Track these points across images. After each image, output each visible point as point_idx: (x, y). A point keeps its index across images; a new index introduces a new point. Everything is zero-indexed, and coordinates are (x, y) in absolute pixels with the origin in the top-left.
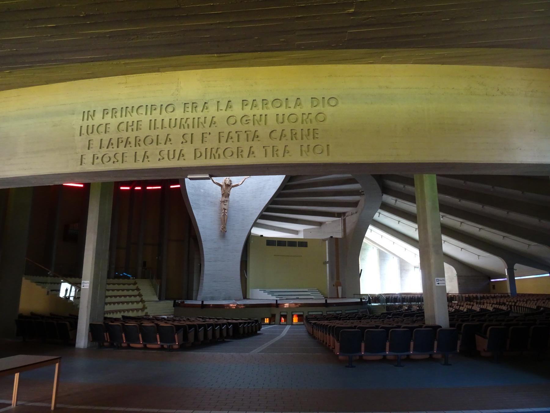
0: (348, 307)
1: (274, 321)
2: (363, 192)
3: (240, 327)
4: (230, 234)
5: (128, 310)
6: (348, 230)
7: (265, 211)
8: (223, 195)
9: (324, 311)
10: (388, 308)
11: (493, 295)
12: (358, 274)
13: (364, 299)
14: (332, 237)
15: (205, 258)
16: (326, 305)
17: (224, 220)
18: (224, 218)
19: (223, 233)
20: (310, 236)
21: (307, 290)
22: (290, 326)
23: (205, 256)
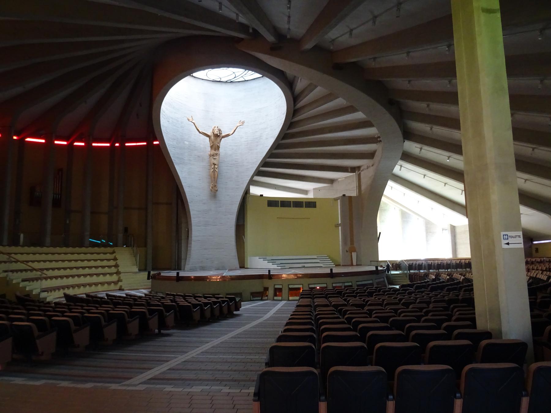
0: (360, 278)
1: (267, 296)
2: (379, 137)
3: (217, 306)
4: (222, 193)
5: (73, 286)
6: (363, 187)
7: (263, 166)
8: (211, 147)
9: (329, 283)
10: (411, 277)
11: (539, 260)
12: (376, 238)
13: (381, 266)
14: (344, 195)
15: (192, 222)
16: (331, 275)
17: (214, 178)
18: (214, 175)
19: (214, 193)
20: (320, 195)
21: (315, 257)
22: (285, 302)
23: (192, 219)
